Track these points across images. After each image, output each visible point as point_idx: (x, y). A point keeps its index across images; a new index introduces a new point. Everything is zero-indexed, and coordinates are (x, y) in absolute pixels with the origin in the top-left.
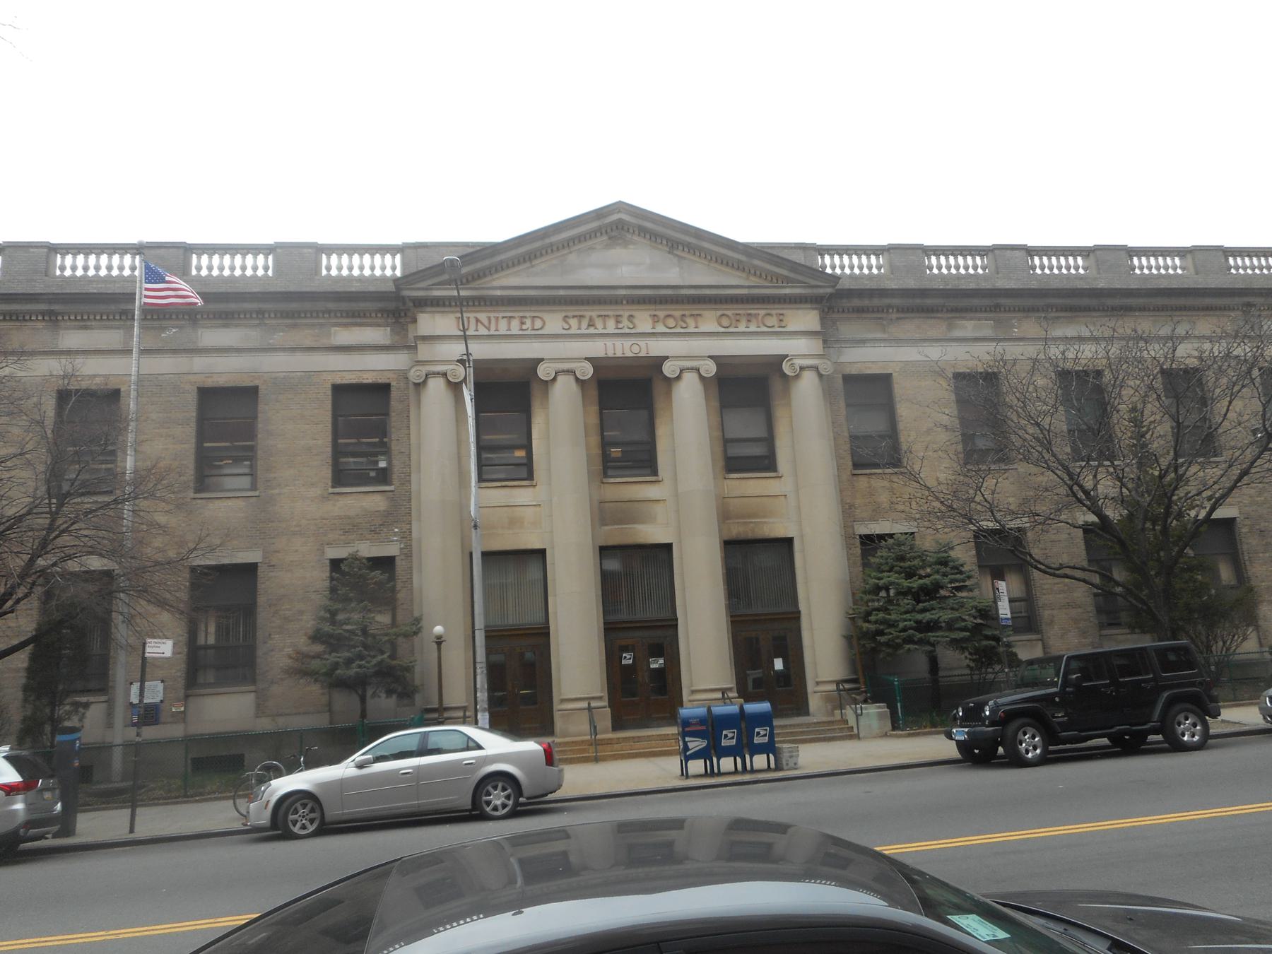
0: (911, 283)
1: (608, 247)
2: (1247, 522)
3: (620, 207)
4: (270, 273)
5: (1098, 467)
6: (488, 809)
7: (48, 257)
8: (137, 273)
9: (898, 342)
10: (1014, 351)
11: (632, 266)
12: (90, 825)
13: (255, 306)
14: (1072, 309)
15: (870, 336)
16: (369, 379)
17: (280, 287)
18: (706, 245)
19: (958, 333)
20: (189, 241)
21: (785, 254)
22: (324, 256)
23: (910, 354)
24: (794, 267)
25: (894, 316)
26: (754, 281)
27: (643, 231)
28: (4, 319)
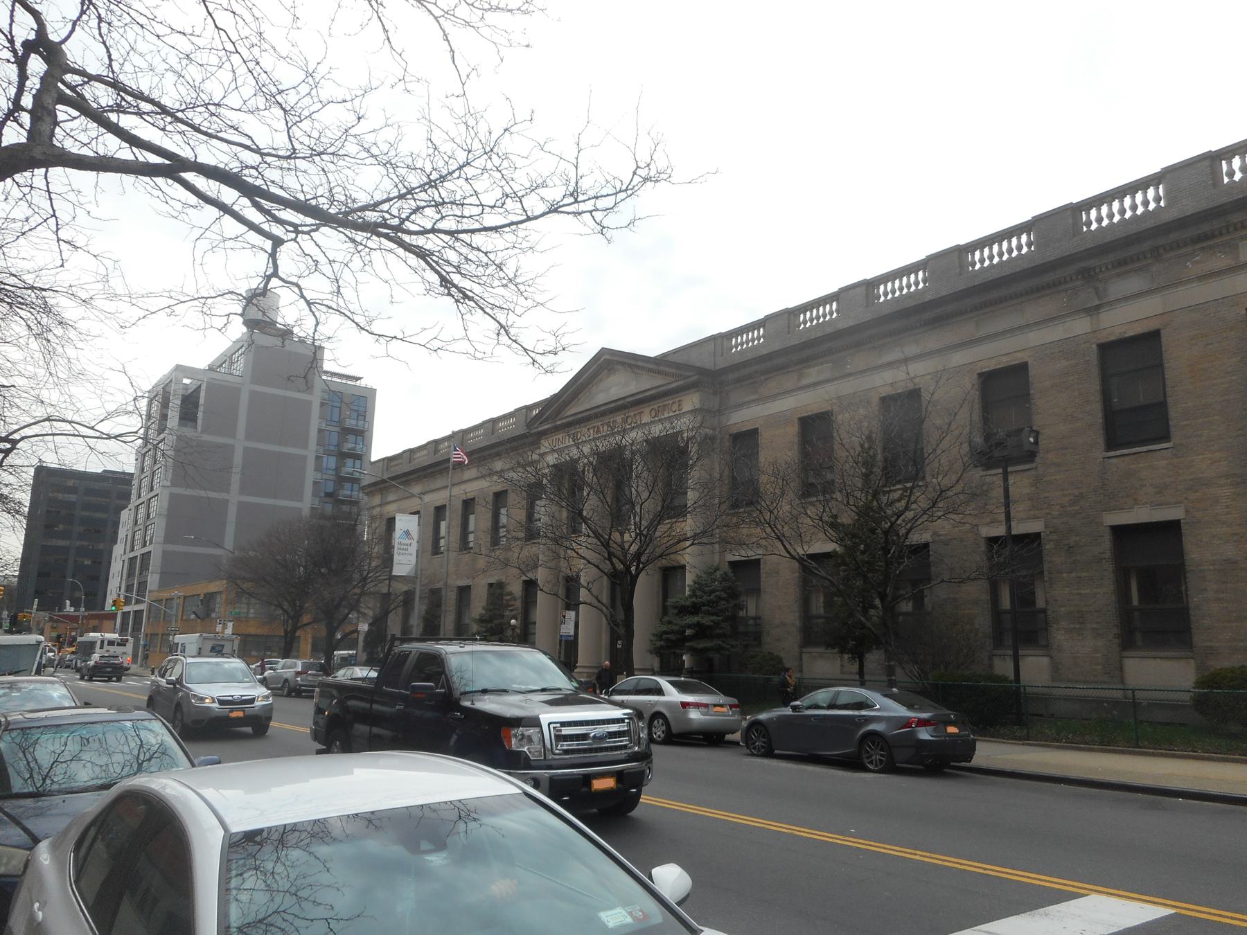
0: (961, 286)
1: (608, 376)
2: (1055, 537)
3: (603, 351)
4: (1162, 204)
5: (913, 487)
6: (866, 761)
7: (1211, 166)
8: (1162, 204)
9: (775, 397)
10: (919, 369)
11: (616, 387)
12: (988, 753)
13: (1146, 246)
14: (1121, 263)
15: (746, 399)
16: (1005, 362)
17: (1175, 214)
18: (640, 363)
19: (805, 382)
20: (868, 277)
21: (670, 359)
22: (1224, 162)
23: (1036, 338)
24: (678, 366)
25: (763, 378)
26: (669, 379)
27: (623, 364)
28: (1242, 222)
